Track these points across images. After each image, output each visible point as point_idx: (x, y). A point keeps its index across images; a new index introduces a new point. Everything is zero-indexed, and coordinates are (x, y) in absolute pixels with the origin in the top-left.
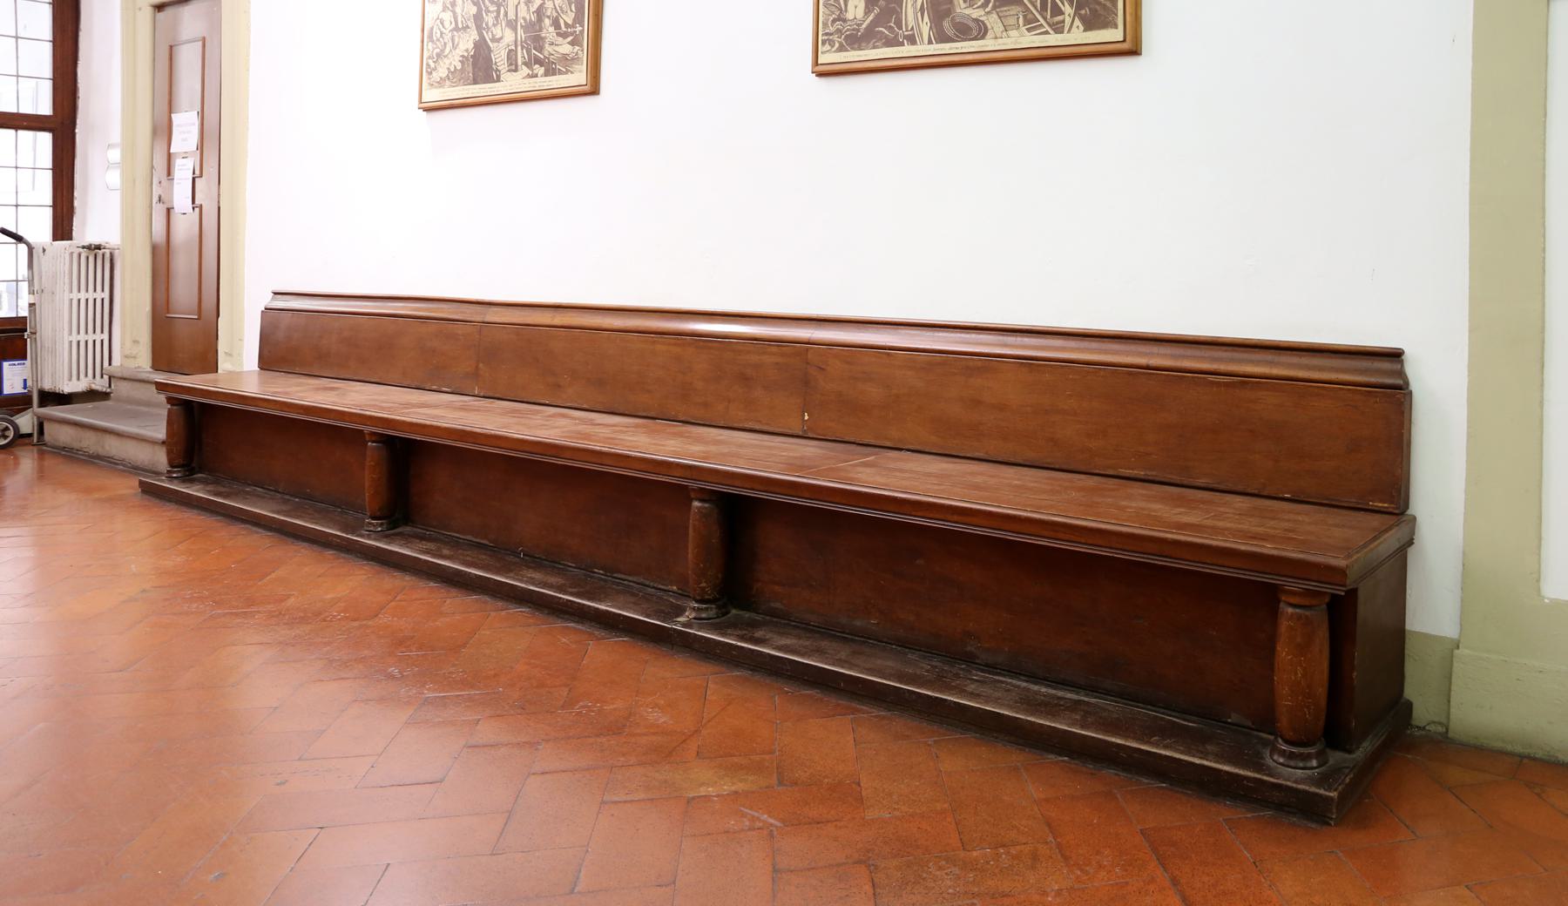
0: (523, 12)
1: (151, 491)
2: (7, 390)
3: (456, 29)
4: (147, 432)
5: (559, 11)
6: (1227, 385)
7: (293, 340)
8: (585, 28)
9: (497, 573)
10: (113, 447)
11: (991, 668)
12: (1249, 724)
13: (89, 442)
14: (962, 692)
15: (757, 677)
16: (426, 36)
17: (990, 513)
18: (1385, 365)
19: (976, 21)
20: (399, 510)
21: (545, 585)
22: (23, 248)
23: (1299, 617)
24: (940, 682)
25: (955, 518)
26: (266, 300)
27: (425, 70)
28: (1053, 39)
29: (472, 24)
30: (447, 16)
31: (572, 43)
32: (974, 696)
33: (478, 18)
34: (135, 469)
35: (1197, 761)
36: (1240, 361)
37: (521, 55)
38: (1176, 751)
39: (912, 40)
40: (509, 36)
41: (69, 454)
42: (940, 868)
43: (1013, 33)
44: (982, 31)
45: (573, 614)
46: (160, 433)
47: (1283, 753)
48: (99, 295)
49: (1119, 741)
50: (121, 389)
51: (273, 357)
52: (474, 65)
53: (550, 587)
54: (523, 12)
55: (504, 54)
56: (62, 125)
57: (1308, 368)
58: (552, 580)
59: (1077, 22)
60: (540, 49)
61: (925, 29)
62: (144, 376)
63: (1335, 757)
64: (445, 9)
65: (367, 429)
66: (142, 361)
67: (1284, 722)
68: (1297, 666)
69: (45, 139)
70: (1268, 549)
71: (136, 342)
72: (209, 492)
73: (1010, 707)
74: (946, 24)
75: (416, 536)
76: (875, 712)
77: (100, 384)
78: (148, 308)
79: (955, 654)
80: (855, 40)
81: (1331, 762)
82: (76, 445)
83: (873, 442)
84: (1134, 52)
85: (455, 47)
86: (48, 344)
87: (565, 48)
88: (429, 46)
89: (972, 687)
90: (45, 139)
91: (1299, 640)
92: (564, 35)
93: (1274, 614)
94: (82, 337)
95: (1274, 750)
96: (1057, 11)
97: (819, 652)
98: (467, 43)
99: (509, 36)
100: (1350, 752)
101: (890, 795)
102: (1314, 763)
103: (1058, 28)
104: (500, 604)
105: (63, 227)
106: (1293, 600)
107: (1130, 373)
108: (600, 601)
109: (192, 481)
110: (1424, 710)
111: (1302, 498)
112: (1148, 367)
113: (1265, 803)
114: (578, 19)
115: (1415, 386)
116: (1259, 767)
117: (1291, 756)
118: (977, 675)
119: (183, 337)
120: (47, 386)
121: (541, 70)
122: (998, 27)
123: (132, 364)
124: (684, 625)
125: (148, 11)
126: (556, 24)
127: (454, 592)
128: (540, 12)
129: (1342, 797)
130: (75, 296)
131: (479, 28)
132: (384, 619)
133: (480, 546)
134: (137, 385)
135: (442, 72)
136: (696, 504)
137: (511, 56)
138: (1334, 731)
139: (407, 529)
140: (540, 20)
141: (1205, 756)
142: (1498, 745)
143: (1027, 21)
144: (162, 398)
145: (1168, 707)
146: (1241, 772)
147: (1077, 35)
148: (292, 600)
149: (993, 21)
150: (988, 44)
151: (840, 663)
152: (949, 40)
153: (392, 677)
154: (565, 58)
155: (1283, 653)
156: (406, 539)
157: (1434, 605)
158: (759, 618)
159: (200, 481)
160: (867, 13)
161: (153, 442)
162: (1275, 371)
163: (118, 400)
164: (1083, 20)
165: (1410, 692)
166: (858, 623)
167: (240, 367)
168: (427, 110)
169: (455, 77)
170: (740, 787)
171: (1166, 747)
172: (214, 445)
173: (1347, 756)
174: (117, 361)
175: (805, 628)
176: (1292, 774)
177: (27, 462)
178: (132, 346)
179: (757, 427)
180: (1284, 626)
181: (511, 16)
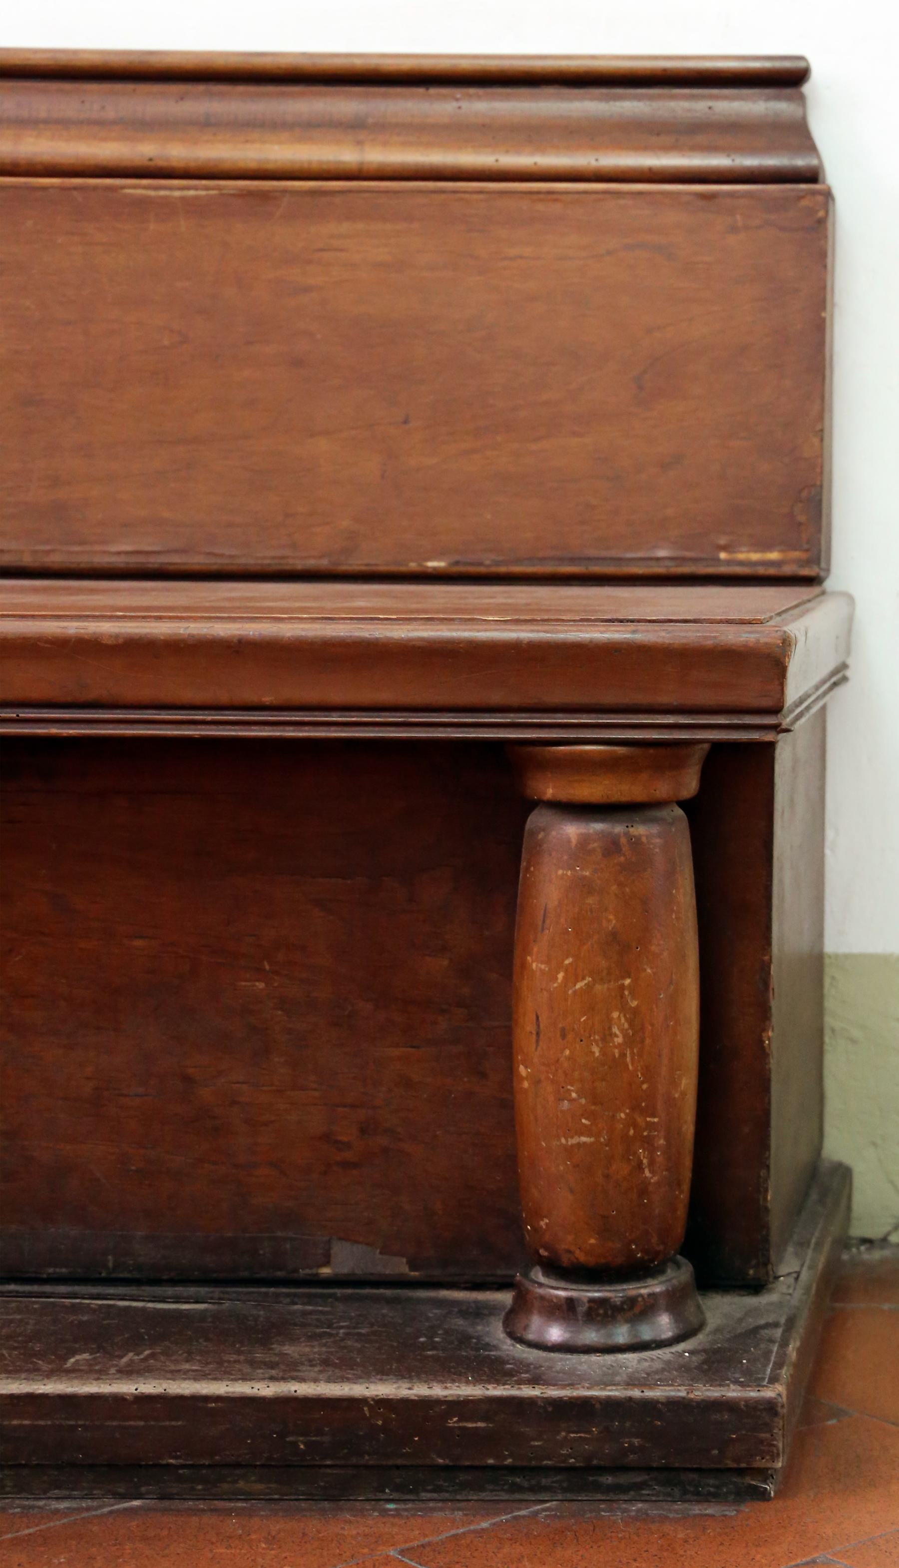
6: (192, 207)
12: (400, 1267)
38: (174, 1375)
47: (566, 1311)
63: (722, 1310)
67: (560, 1211)
81: (713, 1320)
91: (611, 921)
93: (497, 869)
100: (757, 1287)
102: (664, 1324)
111: (489, 563)
115: (836, 176)
116: (497, 1369)
117: (602, 1314)
141: (290, 1370)
146: (437, 1391)
171: (128, 1372)
173: (751, 1301)
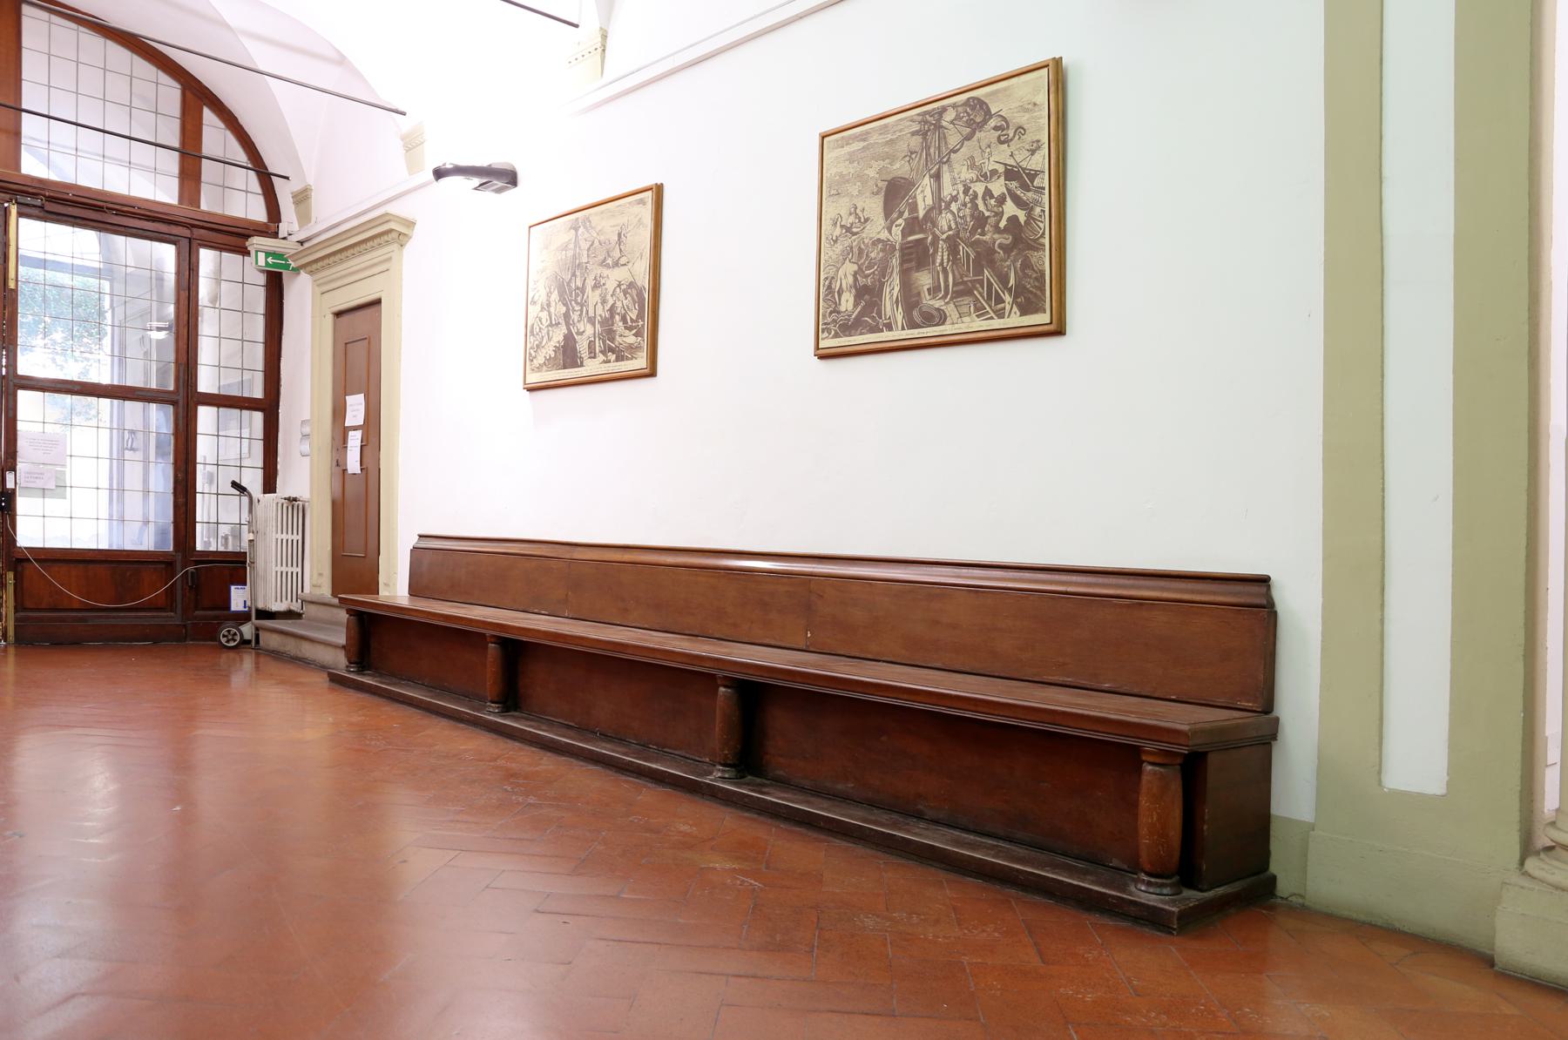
0: (600, 311)
1: (337, 680)
2: (233, 608)
3: (551, 325)
4: (331, 639)
5: (626, 309)
7: (439, 563)
8: (645, 323)
10: (308, 650)
11: (936, 822)
13: (290, 646)
14: (908, 832)
15: (762, 818)
16: (529, 331)
19: (938, 310)
20: (511, 700)
22: (245, 499)
23: (1155, 773)
24: (894, 826)
26: (413, 541)
27: (529, 358)
28: (997, 323)
29: (562, 321)
30: (544, 315)
31: (636, 335)
32: (916, 834)
33: (567, 316)
36: (1140, 588)
37: (598, 345)
39: (889, 327)
40: (589, 330)
41: (277, 655)
43: (966, 319)
44: (942, 319)
46: (342, 640)
48: (295, 537)
50: (310, 611)
51: (414, 591)
52: (564, 353)
54: (600, 311)
55: (586, 344)
56: (269, 406)
57: (1193, 592)
59: (1015, 309)
60: (612, 340)
61: (900, 318)
64: (542, 309)
65: (488, 632)
66: (325, 591)
68: (1155, 806)
69: (258, 417)
70: (1132, 719)
74: (915, 313)
76: (844, 844)
77: (296, 607)
78: (329, 548)
79: (909, 811)
80: (847, 328)
82: (282, 649)
84: (1059, 331)
85: (550, 339)
86: (261, 573)
87: (631, 339)
88: (531, 339)
90: (258, 417)
92: (630, 329)
93: (1138, 770)
94: (284, 569)
95: (1136, 881)
96: (1000, 300)
98: (558, 336)
99: (589, 330)
103: (1001, 316)
105: (269, 486)
106: (1151, 759)
108: (656, 762)
110: (1286, 885)
114: (640, 316)
115: (1279, 607)
116: (1124, 891)
118: (922, 825)
119: (355, 564)
120: (261, 606)
121: (612, 357)
122: (955, 315)
123: (318, 592)
125: (330, 318)
126: (624, 319)
128: (612, 310)
130: (279, 536)
131: (568, 324)
132: (500, 762)
135: (541, 360)
136: (722, 689)
137: (591, 345)
138: (1186, 872)
140: (612, 317)
142: (1346, 913)
143: (977, 310)
144: (343, 615)
145: (1064, 854)
147: (1015, 320)
149: (950, 310)
150: (946, 329)
152: (918, 326)
154: (631, 347)
155: (1144, 802)
156: (516, 719)
157: (1295, 791)
160: (855, 306)
161: (336, 646)
163: (308, 619)
164: (1020, 306)
165: (1274, 868)
166: (840, 787)
167: (395, 588)
168: (530, 390)
169: (550, 363)
170: (736, 866)
172: (382, 647)
174: (307, 590)
175: (801, 789)
176: (1144, 893)
177: (248, 661)
178: (317, 578)
180: (1145, 778)
181: (591, 314)
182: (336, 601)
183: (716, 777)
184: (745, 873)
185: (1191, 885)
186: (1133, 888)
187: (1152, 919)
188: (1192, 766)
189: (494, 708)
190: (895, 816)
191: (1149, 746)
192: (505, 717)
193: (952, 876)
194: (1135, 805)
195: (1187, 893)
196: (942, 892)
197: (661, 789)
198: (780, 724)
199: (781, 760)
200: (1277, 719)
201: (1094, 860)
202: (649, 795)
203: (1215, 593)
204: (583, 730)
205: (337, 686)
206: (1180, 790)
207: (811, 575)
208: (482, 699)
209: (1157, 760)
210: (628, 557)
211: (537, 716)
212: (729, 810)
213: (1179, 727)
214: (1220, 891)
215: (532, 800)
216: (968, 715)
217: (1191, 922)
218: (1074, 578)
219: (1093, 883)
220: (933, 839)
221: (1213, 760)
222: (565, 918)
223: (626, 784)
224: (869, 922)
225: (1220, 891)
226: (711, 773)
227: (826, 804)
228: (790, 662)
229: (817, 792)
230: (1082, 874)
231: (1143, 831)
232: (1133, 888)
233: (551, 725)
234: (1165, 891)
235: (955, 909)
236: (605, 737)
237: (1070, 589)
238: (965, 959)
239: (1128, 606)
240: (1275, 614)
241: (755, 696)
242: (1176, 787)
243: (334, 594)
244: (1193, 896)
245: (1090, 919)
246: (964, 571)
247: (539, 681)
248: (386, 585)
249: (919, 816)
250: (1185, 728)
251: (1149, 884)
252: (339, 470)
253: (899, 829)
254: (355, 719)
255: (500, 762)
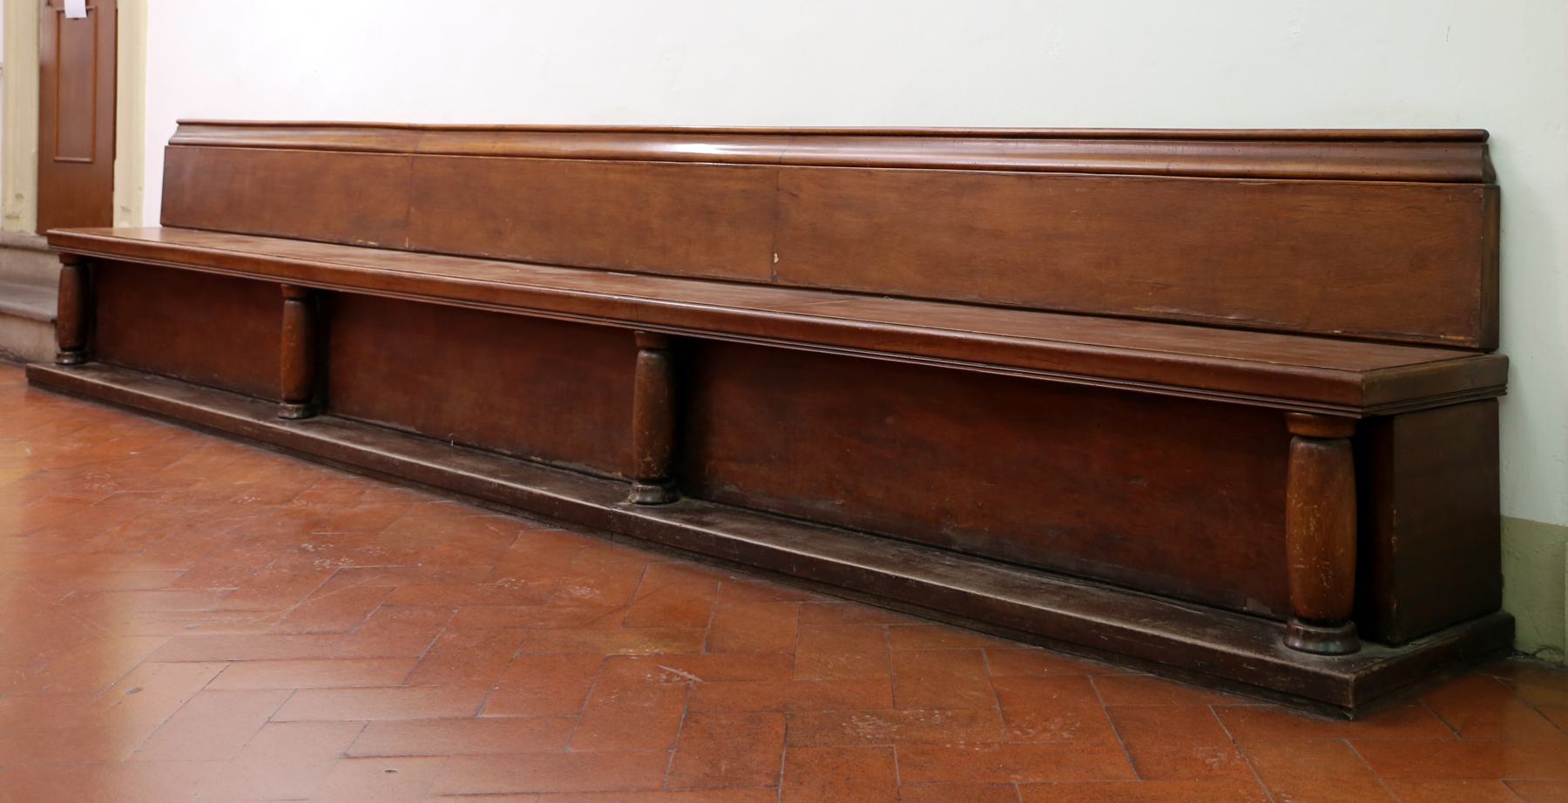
1: (41, 381)
7: (213, 170)
9: (424, 457)
11: (969, 554)
12: (1267, 611)
14: (927, 573)
17: (960, 341)
18: (1473, 153)
20: (316, 397)
21: (475, 470)
23: (1310, 453)
24: (907, 564)
25: (922, 350)
26: (169, 132)
32: (939, 577)
34: (19, 361)
35: (1189, 641)
42: (864, 720)
45: (503, 504)
46: (50, 309)
49: (1099, 620)
51: (171, 217)
53: (481, 472)
58: (485, 466)
62: (28, 242)
65: (285, 281)
68: (1312, 512)
70: (1272, 367)
71: (19, 197)
72: (105, 379)
73: (980, 587)
75: (335, 425)
76: (829, 600)
78: (33, 149)
79: (926, 538)
83: (851, 288)
89: (940, 570)
93: (1285, 452)
97: (774, 536)
101: (826, 664)
104: (425, 496)
106: (1302, 430)
107: (1147, 182)
108: (535, 485)
109: (86, 369)
112: (1168, 173)
113: (1267, 692)
115: (1504, 181)
118: (949, 560)
124: (625, 508)
127: (375, 484)
129: (1361, 686)
132: (297, 504)
133: (406, 434)
134: (20, 254)
136: (643, 354)
138: (1363, 612)
139: (325, 418)
144: (54, 266)
146: (1240, 652)
148: (200, 485)
151: (795, 545)
153: (305, 551)
156: (324, 427)
158: (712, 506)
159: (94, 369)
162: (1322, 169)
165: (1512, 603)
166: (822, 506)
167: (139, 214)
175: (762, 514)
176: (1299, 653)
179: (721, 275)
180: (1296, 462)
182: (43, 242)
183: (633, 504)
184: (672, 660)
185: (1374, 638)
186: (1280, 646)
187: (1310, 696)
188: (1370, 437)
189: (291, 411)
190: (908, 549)
191: (1300, 410)
192: (306, 426)
193: (998, 643)
194: (1280, 508)
195: (1369, 649)
196: (980, 671)
197: (547, 529)
198: (733, 406)
199: (733, 466)
200: (1505, 361)
201: (1216, 602)
202: (527, 542)
203: (1399, 163)
204: (430, 438)
205: (41, 392)
206: (1351, 480)
207: (780, 162)
208: (273, 398)
209: (1313, 431)
210: (501, 145)
211: (358, 422)
212: (652, 556)
213: (1346, 377)
214: (1422, 644)
215: (345, 563)
216: (1018, 374)
217: (1375, 699)
218: (1180, 149)
219: (1216, 639)
220: (966, 583)
221: (1404, 430)
222: (390, 764)
223: (492, 527)
224: (866, 728)
225: (1422, 644)
226: (624, 497)
227: (801, 536)
228: (745, 305)
229: (789, 518)
230: (1198, 626)
231: (1295, 550)
232: (1280, 646)
233: (379, 434)
234: (1333, 647)
235: (999, 696)
236: (464, 448)
237: (1174, 166)
238: (1016, 779)
239: (1263, 190)
240: (1497, 191)
241: (695, 361)
242: (1344, 476)
243: (41, 231)
244: (1377, 654)
245: (1216, 701)
246: (1012, 145)
247: (364, 359)
248: (125, 210)
249: (945, 547)
250: (1357, 378)
251: (1307, 636)
252: (50, 13)
253: (913, 570)
254: (69, 446)
255: (297, 504)
